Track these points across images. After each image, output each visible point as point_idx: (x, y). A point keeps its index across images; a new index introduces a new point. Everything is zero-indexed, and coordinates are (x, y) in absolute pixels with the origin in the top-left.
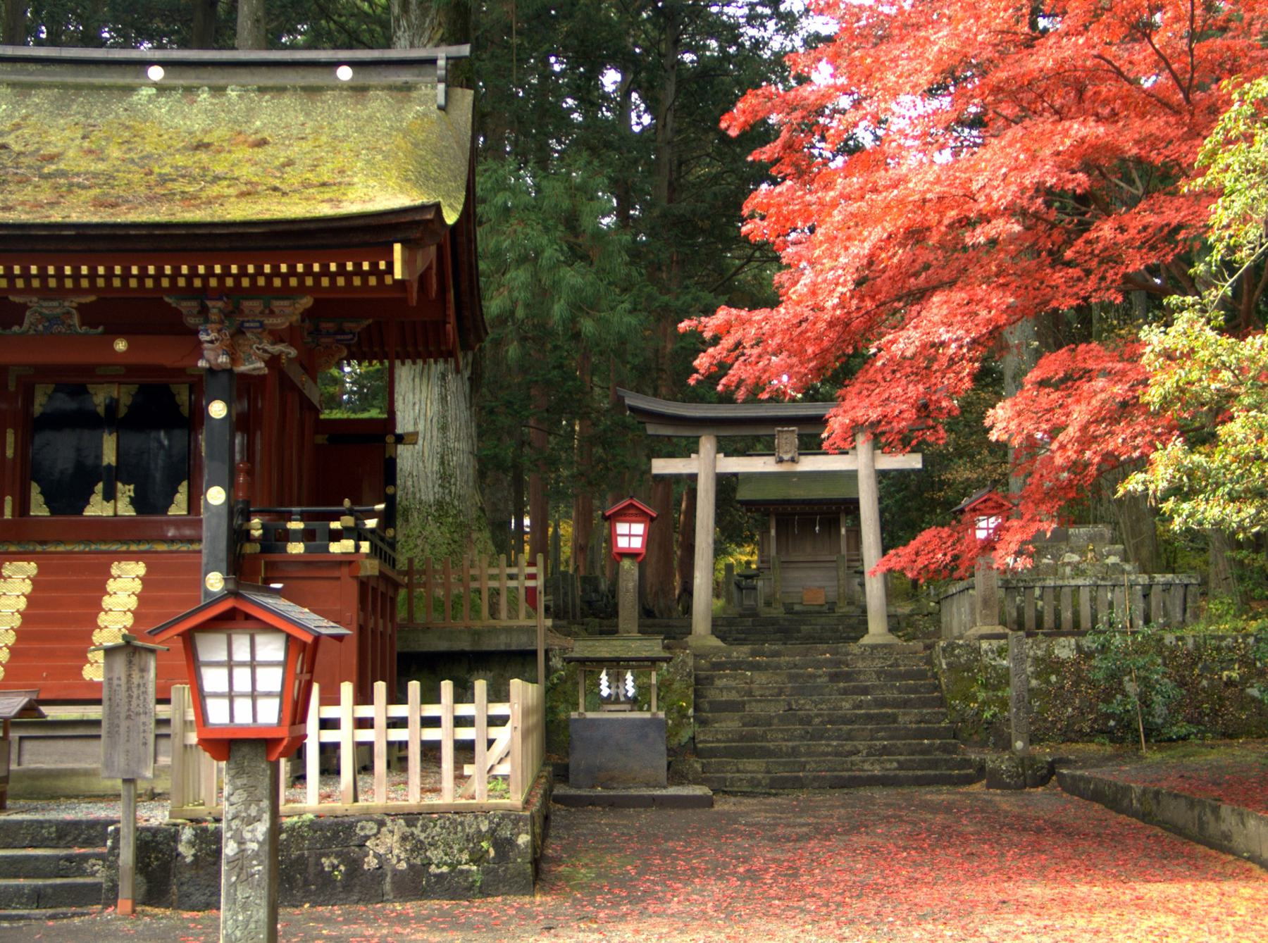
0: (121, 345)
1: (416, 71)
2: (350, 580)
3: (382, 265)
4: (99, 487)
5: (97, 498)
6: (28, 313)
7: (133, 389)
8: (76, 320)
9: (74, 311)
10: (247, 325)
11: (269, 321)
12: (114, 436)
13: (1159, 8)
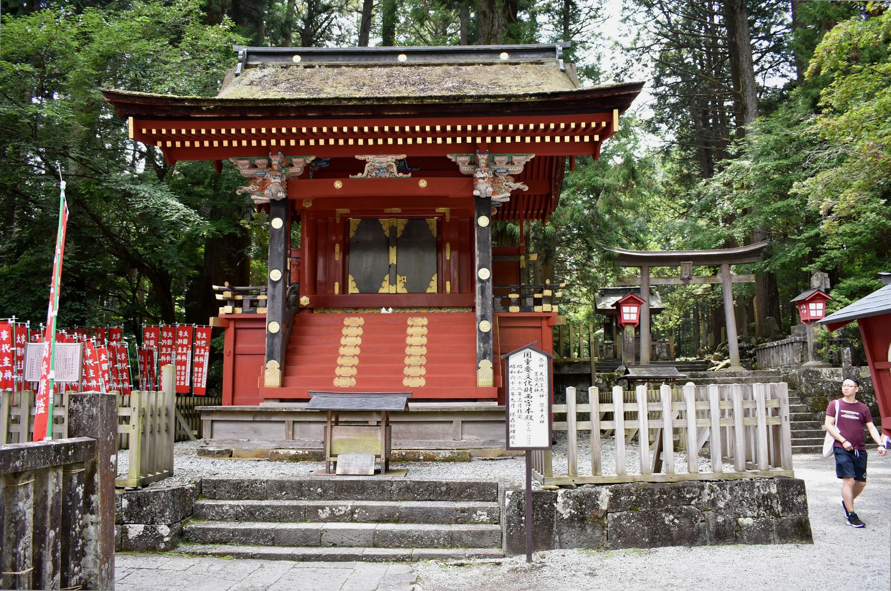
0: (423, 183)
1: (436, 57)
2: (548, 328)
3: (604, 124)
4: (387, 278)
5: (386, 284)
6: (367, 165)
7: (405, 221)
8: (395, 169)
9: (394, 164)
10: (498, 171)
12: (395, 248)
13: (866, 3)
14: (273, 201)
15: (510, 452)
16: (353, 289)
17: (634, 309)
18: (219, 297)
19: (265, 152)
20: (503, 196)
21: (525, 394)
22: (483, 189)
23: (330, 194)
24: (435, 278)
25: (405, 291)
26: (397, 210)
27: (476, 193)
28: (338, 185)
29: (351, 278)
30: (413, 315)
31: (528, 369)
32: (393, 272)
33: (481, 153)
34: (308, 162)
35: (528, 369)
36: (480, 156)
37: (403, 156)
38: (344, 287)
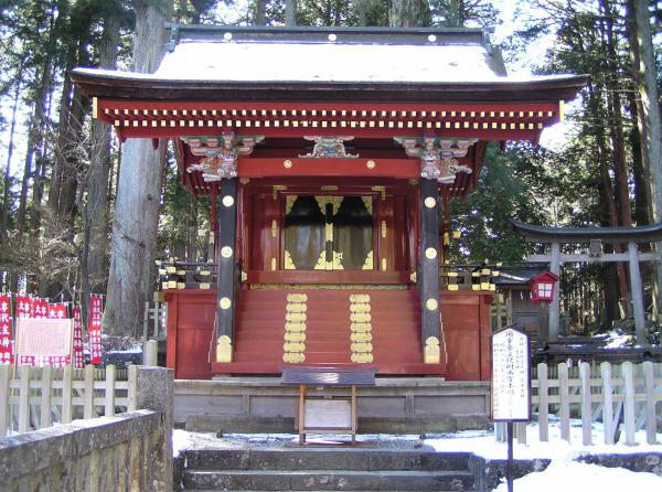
0: (371, 164)
3: (550, 114)
7: (341, 199)
8: (343, 150)
11: (456, 152)
14: (223, 179)
15: (486, 423)
16: (289, 264)
17: (549, 286)
18: (162, 272)
19: (216, 131)
20: (449, 178)
21: (507, 370)
22: (430, 170)
23: (281, 173)
24: (371, 254)
25: (341, 267)
26: (335, 188)
27: (424, 175)
28: (288, 164)
29: (287, 254)
30: (293, 292)
31: (510, 348)
32: (332, 248)
33: (226, 134)
34: (258, 141)
35: (510, 348)
36: (225, 138)
37: (351, 138)
38: (280, 264)
